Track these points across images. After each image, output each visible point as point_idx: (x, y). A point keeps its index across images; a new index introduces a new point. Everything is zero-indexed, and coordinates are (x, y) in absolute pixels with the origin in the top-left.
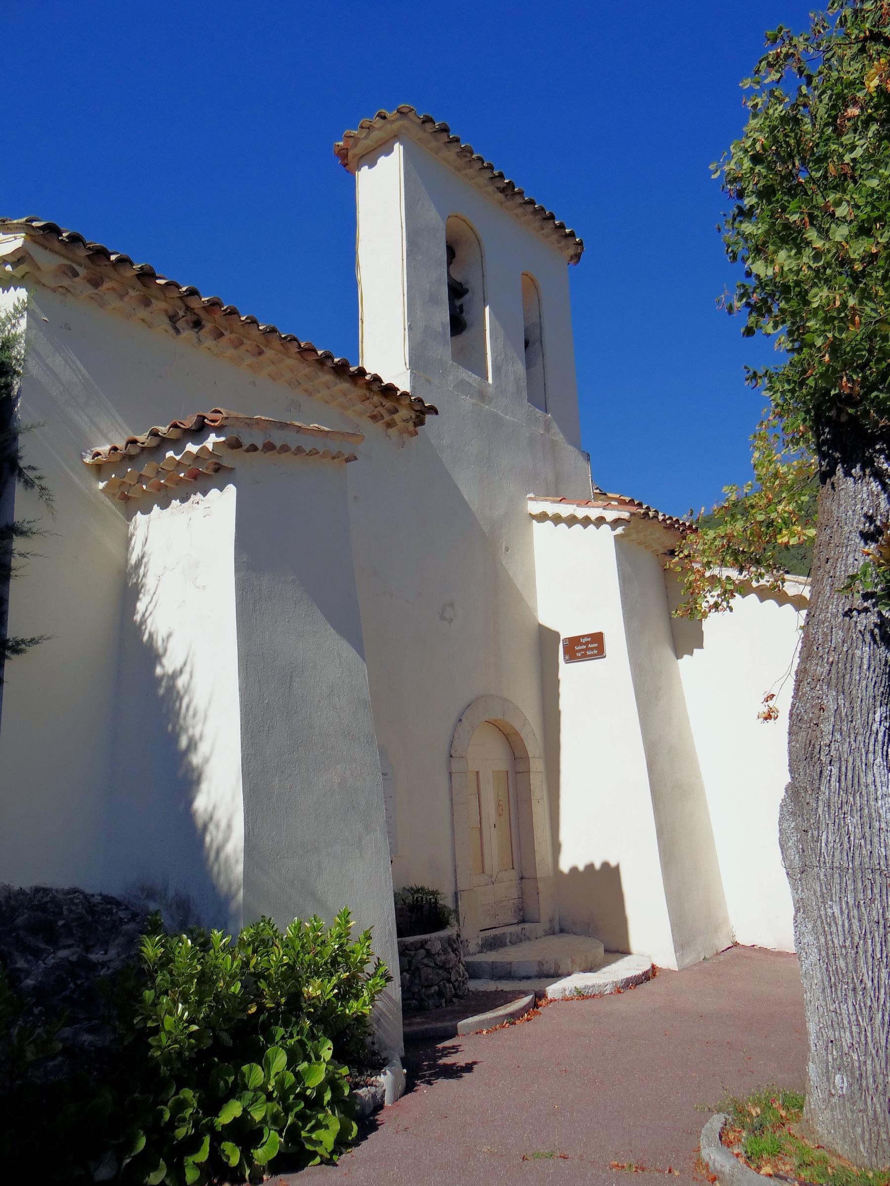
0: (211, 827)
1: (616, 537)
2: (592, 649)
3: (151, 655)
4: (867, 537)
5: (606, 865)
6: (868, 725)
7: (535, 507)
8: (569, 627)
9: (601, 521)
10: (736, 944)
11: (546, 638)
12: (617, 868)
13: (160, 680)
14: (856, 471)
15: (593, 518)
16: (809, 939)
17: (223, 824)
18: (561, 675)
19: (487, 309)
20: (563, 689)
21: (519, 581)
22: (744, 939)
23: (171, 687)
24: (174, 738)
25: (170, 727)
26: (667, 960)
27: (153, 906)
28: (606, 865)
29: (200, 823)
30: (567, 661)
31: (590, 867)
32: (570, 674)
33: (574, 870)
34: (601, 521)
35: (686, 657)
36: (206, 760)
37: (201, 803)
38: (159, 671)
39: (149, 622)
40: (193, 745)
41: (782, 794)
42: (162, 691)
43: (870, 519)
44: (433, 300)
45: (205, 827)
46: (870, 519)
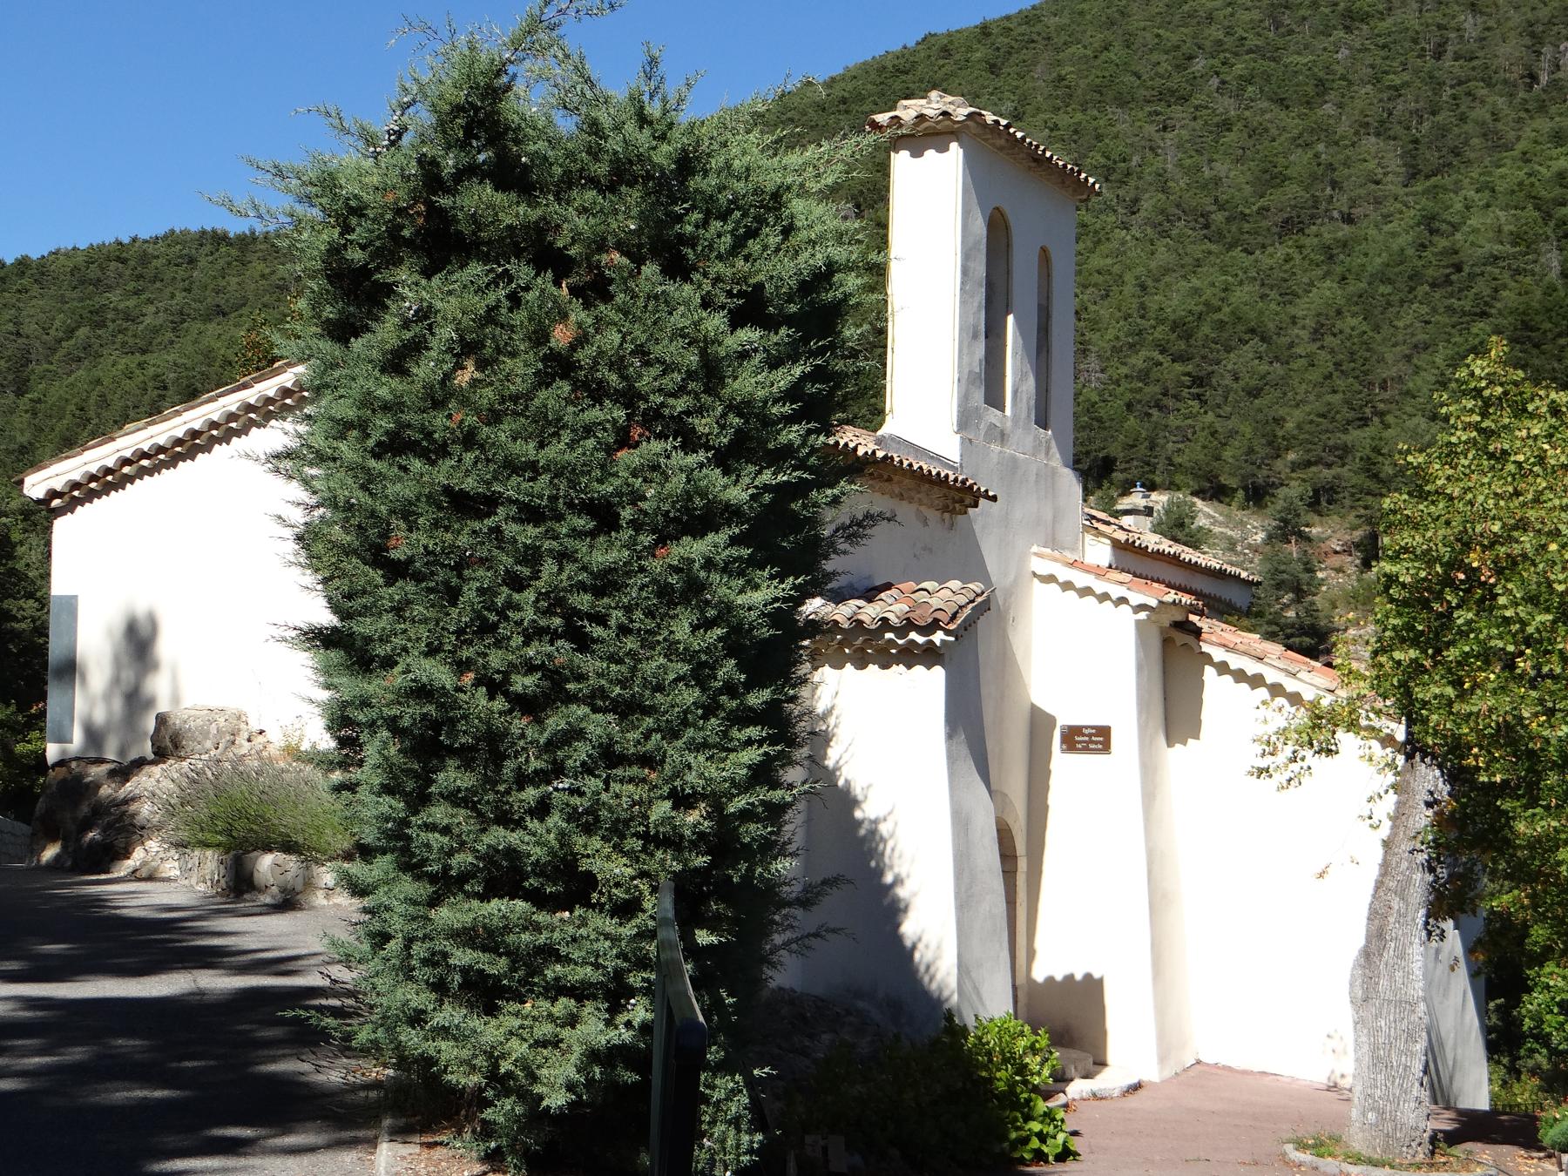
0: (920, 946)
1: (1138, 622)
2: (1096, 743)
3: (847, 801)
4: (1429, 805)
5: (1088, 977)
6: (1414, 920)
7: (1044, 567)
8: (1067, 715)
9: (1123, 600)
10: (1199, 1062)
11: (1039, 723)
12: (1101, 981)
13: (859, 823)
14: (1428, 760)
15: (1114, 597)
16: (1364, 1039)
17: (933, 946)
18: (1053, 766)
19: (1010, 319)
20: (1054, 782)
21: (1019, 658)
22: (1207, 1058)
23: (873, 832)
24: (880, 872)
25: (873, 864)
26: (1150, 1073)
27: (861, 1004)
28: (1088, 977)
29: (908, 943)
30: (1063, 751)
31: (1070, 978)
32: (1064, 766)
33: (1050, 980)
34: (1123, 600)
35: (1178, 746)
36: (915, 894)
37: (909, 928)
38: (858, 814)
39: (844, 770)
40: (898, 881)
41: (1356, 953)
42: (862, 832)
43: (1431, 793)
44: (975, 336)
45: (914, 947)
46: (1431, 793)
